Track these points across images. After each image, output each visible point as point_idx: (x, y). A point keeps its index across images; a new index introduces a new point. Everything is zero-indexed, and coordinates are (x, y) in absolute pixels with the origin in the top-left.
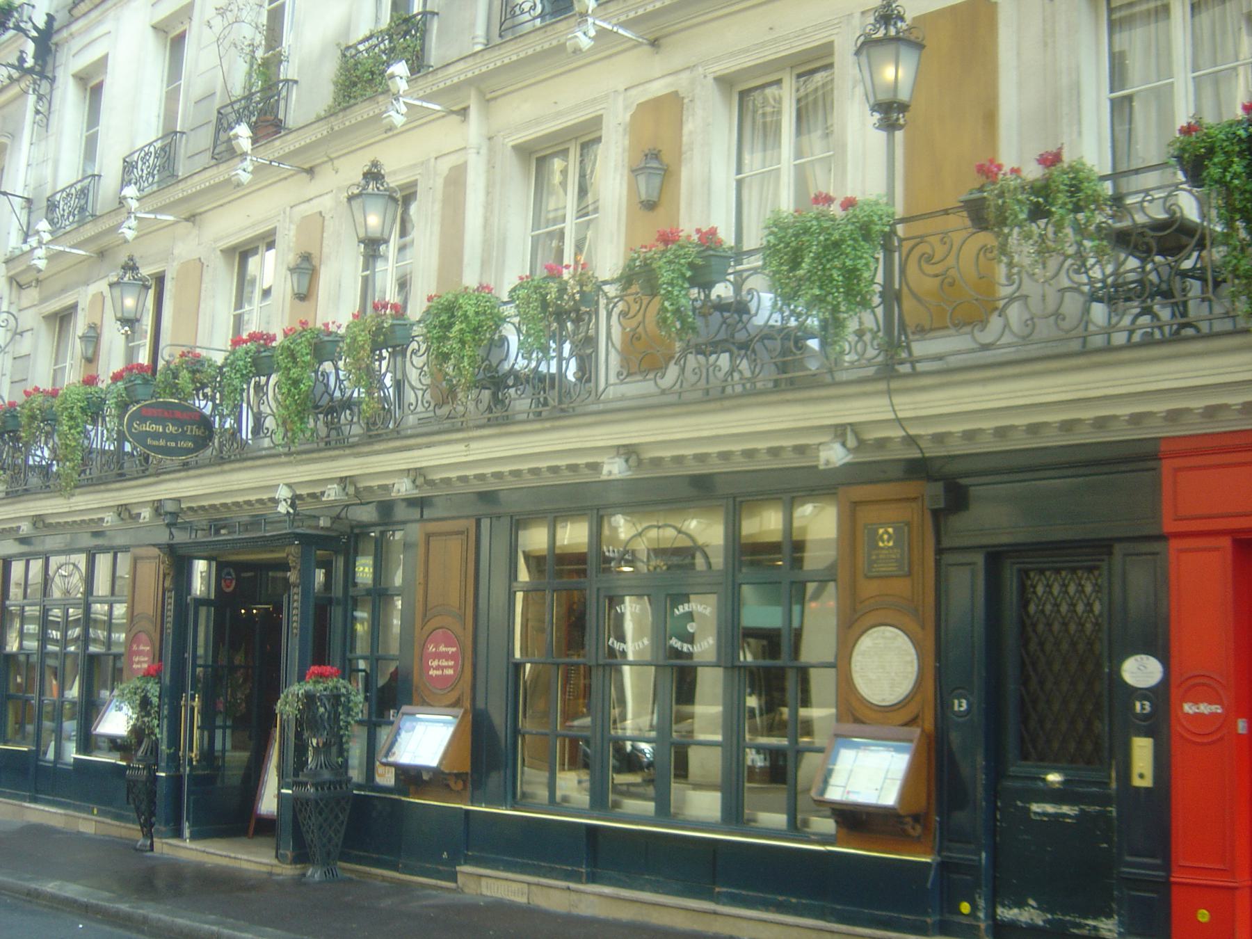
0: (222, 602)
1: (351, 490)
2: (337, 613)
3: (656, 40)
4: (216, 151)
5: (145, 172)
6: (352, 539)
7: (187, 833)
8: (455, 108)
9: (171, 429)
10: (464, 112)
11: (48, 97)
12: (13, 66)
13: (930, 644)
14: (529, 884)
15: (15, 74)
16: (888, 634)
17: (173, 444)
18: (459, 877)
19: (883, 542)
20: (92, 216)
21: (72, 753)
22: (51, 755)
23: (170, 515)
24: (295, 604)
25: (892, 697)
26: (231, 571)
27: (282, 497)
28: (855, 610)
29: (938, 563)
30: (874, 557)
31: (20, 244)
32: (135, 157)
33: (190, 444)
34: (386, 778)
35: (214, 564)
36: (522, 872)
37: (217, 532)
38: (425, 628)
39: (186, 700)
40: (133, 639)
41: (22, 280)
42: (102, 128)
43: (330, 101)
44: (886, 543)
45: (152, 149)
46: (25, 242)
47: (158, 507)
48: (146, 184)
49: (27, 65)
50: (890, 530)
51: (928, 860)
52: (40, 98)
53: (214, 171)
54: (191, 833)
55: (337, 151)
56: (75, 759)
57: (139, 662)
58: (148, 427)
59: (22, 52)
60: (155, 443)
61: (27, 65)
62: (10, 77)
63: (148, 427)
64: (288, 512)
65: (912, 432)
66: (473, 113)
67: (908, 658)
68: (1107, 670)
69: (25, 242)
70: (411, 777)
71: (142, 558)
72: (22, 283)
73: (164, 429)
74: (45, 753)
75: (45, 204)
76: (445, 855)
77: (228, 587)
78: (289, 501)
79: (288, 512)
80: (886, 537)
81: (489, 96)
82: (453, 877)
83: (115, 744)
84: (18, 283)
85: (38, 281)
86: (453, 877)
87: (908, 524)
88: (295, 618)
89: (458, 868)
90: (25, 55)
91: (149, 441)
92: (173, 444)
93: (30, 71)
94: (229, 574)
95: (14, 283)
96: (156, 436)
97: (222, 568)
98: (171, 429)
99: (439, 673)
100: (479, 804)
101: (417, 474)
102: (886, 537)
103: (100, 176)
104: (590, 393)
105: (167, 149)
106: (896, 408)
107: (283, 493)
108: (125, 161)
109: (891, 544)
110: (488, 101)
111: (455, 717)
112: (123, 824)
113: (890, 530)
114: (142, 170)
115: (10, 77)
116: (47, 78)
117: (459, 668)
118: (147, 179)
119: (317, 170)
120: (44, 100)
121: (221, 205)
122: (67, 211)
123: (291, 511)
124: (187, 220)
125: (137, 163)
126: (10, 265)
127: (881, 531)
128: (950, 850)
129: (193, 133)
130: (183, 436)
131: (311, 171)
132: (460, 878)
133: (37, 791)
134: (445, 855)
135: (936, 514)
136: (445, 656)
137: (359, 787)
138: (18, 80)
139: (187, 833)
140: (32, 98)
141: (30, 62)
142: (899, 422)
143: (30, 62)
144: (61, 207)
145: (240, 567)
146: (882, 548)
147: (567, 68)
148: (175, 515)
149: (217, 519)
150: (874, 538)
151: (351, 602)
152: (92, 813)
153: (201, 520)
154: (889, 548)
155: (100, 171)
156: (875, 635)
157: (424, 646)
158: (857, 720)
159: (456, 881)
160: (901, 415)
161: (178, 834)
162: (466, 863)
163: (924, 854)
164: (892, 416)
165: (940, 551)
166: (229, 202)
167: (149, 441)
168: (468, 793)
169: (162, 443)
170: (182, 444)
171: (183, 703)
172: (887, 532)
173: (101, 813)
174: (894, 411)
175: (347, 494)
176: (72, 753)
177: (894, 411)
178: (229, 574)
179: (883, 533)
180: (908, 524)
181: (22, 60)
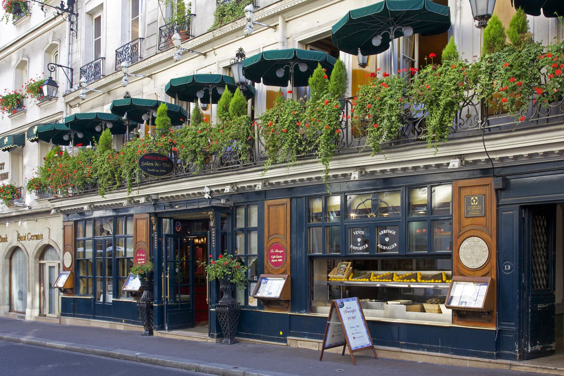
0: (176, 236)
1: (236, 188)
2: (229, 239)
3: (109, 91)
4: (160, 47)
5: (127, 56)
6: (234, 209)
7: (167, 328)
8: (272, 25)
9: (157, 164)
10: (275, 27)
11: (76, 23)
12: (58, 8)
13: (494, 243)
14: (319, 342)
15: (60, 12)
16: (475, 240)
17: (158, 171)
18: (288, 340)
19: (473, 203)
20: (103, 76)
21: (110, 298)
22: (101, 300)
23: (156, 202)
24: (213, 235)
25: (477, 265)
26: (179, 223)
27: (206, 192)
28: (460, 231)
29: (497, 210)
30: (469, 209)
31: (69, 89)
32: (85, 68)
33: (165, 171)
34: (253, 303)
35: (172, 220)
36: (315, 338)
37: (171, 206)
38: (269, 243)
39: (164, 275)
40: (137, 251)
41: (72, 104)
42: (103, 37)
43: (213, 24)
44: (474, 203)
45: (129, 46)
46: (71, 87)
47: (148, 197)
48: (91, 79)
49: (65, 8)
50: (476, 198)
51: (494, 329)
52: (72, 23)
53: (161, 55)
54: (168, 328)
55: (217, 45)
56: (113, 301)
57: (140, 261)
58: (147, 164)
59: (62, 2)
60: (151, 170)
61: (65, 8)
62: (58, 13)
63: (147, 164)
64: (209, 198)
65: (491, 157)
66: (280, 27)
67: (485, 249)
68: (223, 201)
69: (71, 87)
70: (266, 302)
71: (140, 219)
72: (71, 105)
73: (154, 164)
74: (99, 299)
75: (79, 71)
76: (281, 333)
77: (178, 229)
78: (209, 193)
79: (209, 198)
80: (474, 201)
81: (287, 20)
82: (285, 341)
83: (132, 294)
84: (70, 105)
85: (79, 104)
86: (285, 341)
87: (485, 195)
88: (213, 241)
89: (288, 338)
90: (63, 3)
91: (148, 170)
92: (158, 171)
93: (67, 11)
94: (178, 224)
95: (68, 106)
96: (151, 167)
97: (175, 222)
98: (157, 164)
99: (276, 261)
100: (295, 312)
101: (265, 181)
102: (474, 201)
103: (105, 58)
104: (344, 144)
105: (137, 45)
106: (486, 147)
107: (207, 190)
108: (116, 51)
109: (477, 203)
110: (287, 22)
111: (285, 279)
112: (137, 326)
113: (476, 198)
114: (125, 55)
115: (58, 13)
116: (74, 14)
117: (285, 258)
118: (91, 76)
119: (207, 54)
120: (74, 24)
121: (164, 70)
122: (90, 74)
123: (210, 197)
124: (149, 77)
125: (123, 52)
126: (66, 97)
127: (472, 198)
128: (502, 325)
129: (148, 38)
130: (162, 167)
131: (205, 54)
132: (288, 341)
133: (95, 314)
134: (281, 333)
135: (497, 190)
136: (279, 254)
137: (242, 307)
138: (62, 14)
139: (167, 328)
140: (67, 23)
141: (66, 7)
142: (487, 153)
143: (66, 7)
144: (88, 72)
145: (183, 221)
146: (473, 205)
147: (192, 57)
148: (156, 200)
149: (172, 202)
150: (469, 202)
151: (234, 234)
152: (122, 322)
153: (166, 203)
154: (476, 205)
155: (106, 55)
156: (469, 240)
157: (269, 250)
158: (462, 275)
159: (286, 342)
160: (487, 150)
161: (163, 328)
162: (290, 335)
163: (492, 327)
164: (484, 150)
165: (498, 206)
166: (294, 19)
167: (148, 170)
168: (289, 308)
169: (153, 170)
170: (162, 171)
171: (162, 276)
172: (475, 199)
173: (126, 322)
174: (485, 148)
175: (234, 190)
176: (110, 298)
177: (485, 148)
178: (178, 224)
179: (473, 199)
180: (485, 195)
181: (62, 5)
